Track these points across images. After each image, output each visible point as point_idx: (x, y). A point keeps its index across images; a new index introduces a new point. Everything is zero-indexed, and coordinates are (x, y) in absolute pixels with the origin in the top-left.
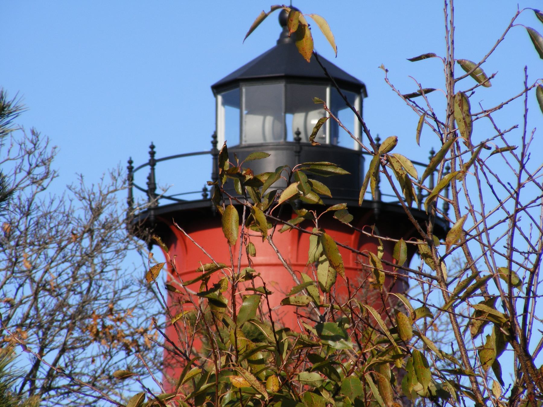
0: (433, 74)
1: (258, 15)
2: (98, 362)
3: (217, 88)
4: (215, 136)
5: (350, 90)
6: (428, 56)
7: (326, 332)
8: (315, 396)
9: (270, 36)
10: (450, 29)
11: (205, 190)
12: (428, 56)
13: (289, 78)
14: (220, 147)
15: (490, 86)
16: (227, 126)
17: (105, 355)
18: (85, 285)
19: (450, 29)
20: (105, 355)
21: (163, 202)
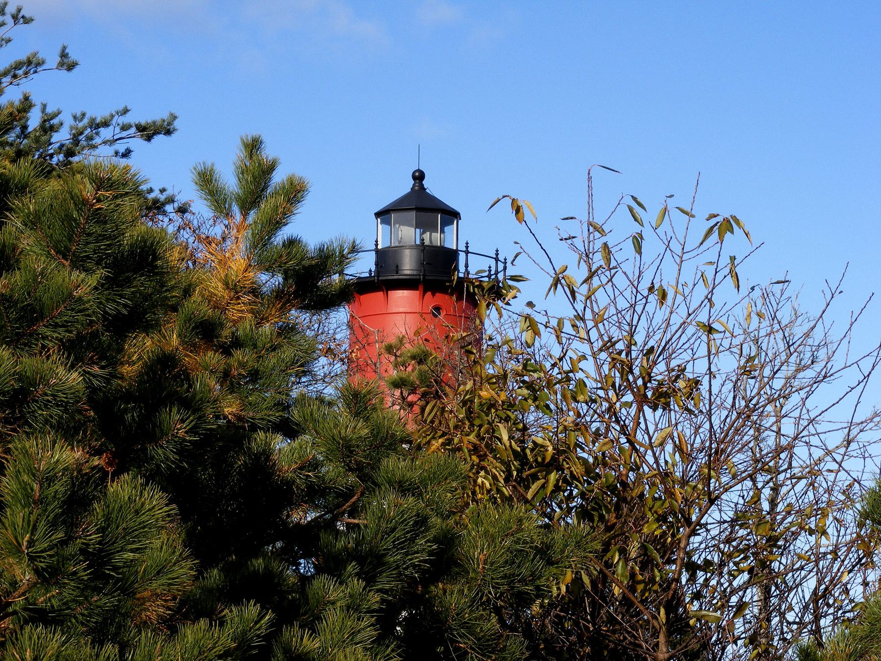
0: (577, 229)
1: (495, 199)
2: (326, 367)
3: (378, 215)
4: (377, 241)
5: (451, 215)
6: (572, 218)
7: (529, 368)
8: (524, 402)
9: (406, 186)
10: (590, 204)
11: (370, 271)
12: (572, 218)
13: (418, 209)
14: (380, 247)
15: (175, 130)
16: (383, 236)
17: (330, 364)
18: (316, 326)
19: (590, 204)
20: (330, 364)
21: (347, 278)
